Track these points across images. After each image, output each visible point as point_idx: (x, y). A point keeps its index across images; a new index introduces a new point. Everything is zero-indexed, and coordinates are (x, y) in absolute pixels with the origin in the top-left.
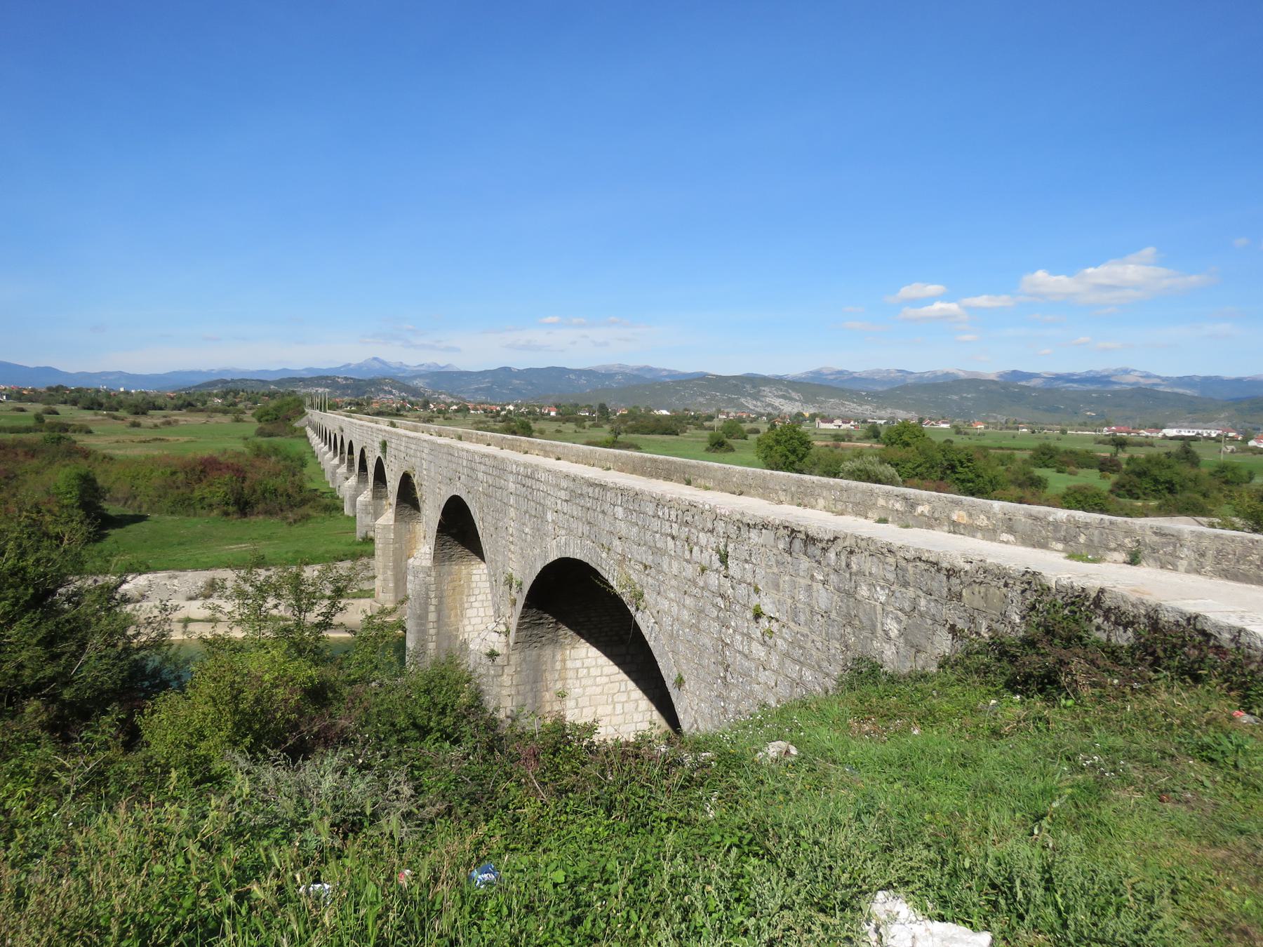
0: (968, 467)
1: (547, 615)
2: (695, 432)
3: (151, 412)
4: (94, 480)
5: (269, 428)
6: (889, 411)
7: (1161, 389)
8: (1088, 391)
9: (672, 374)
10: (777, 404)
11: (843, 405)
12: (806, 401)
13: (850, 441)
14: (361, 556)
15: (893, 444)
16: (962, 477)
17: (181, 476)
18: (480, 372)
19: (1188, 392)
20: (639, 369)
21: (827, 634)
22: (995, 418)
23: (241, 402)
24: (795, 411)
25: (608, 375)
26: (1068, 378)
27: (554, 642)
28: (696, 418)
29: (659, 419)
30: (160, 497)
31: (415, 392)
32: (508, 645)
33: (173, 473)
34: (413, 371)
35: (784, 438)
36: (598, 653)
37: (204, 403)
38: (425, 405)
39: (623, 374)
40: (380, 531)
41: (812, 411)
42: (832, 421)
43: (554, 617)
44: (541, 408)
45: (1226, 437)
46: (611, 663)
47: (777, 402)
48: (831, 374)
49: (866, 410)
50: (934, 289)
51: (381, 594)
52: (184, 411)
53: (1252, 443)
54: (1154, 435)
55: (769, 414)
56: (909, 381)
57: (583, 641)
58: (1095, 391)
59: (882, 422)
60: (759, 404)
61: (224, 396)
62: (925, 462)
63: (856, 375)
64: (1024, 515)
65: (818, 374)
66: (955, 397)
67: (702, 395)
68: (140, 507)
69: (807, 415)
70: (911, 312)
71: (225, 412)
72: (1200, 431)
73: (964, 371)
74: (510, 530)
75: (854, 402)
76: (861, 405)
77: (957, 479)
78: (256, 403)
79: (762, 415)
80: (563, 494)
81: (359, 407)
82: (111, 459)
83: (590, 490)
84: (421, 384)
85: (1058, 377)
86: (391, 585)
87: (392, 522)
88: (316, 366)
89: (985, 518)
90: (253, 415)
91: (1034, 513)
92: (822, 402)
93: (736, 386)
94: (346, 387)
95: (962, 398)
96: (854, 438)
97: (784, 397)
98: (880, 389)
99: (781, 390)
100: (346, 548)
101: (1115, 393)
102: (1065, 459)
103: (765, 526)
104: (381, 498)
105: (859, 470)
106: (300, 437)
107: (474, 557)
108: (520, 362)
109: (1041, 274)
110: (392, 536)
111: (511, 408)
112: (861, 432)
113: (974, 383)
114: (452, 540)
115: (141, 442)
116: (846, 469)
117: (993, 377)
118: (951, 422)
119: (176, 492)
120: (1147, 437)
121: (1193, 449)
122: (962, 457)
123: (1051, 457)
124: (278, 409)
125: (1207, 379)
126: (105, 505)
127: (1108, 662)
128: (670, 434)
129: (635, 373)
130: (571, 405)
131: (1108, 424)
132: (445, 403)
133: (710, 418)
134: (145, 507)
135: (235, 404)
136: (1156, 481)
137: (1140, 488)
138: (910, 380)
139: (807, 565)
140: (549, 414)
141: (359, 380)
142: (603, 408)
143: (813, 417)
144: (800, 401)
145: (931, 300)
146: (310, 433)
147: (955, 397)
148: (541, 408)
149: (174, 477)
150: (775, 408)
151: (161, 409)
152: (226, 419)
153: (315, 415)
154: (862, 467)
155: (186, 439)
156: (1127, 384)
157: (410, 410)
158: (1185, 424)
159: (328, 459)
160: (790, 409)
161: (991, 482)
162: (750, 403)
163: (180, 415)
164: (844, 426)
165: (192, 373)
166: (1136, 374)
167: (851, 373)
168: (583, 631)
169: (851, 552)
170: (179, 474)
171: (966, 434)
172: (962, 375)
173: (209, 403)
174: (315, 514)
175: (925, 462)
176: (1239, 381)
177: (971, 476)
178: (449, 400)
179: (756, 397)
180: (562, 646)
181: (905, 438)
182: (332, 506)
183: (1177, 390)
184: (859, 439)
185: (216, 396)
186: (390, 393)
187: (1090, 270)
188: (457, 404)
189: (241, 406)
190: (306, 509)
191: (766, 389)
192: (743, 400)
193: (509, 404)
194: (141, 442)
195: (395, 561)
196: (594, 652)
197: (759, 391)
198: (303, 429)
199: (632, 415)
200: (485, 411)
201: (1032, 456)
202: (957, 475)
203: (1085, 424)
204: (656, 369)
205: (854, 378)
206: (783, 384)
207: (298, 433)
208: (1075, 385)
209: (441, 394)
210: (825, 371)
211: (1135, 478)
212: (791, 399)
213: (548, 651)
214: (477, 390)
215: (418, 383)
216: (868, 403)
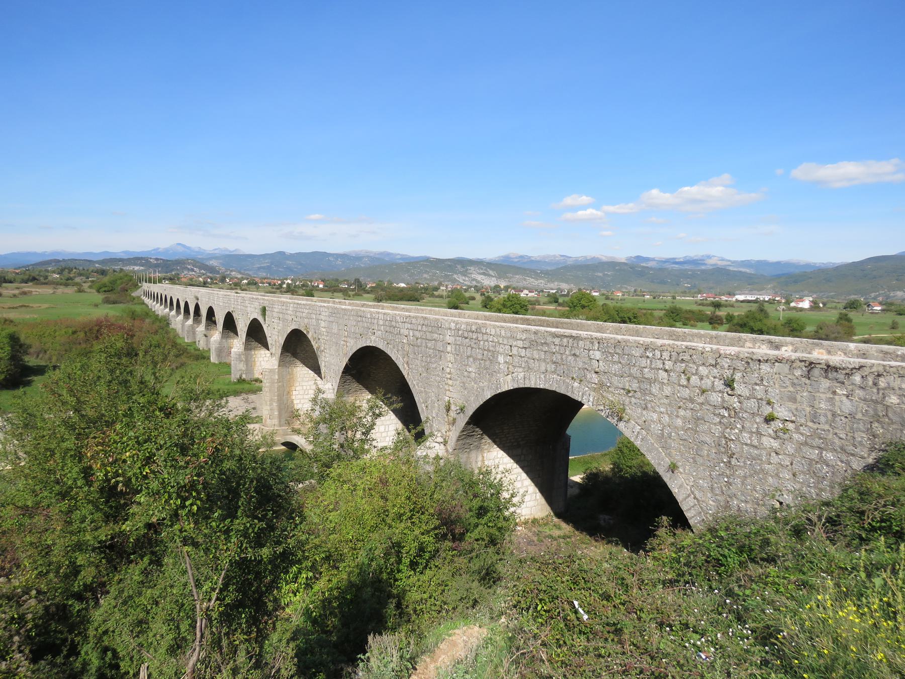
1: (477, 429)
2: (430, 299)
3: (4, 285)
4: (18, 339)
5: (112, 296)
6: (556, 283)
7: (731, 268)
8: (686, 269)
9: (404, 258)
10: (479, 279)
11: (525, 280)
12: (499, 277)
13: (539, 305)
14: (241, 392)
15: (575, 306)
17: (81, 335)
18: (261, 255)
19: (748, 271)
20: (381, 253)
21: (852, 428)
22: (626, 288)
23: (75, 277)
24: (493, 284)
25: (358, 258)
26: (674, 261)
27: (478, 448)
28: (426, 289)
29: (402, 290)
30: (66, 351)
31: (212, 269)
32: (447, 451)
33: (74, 333)
34: (209, 254)
35: (509, 304)
36: (505, 455)
37: (46, 277)
38: (223, 280)
39: (368, 257)
40: (267, 373)
43: (482, 430)
44: (311, 282)
45: (774, 300)
46: (512, 461)
47: (479, 278)
49: (541, 283)
50: (585, 199)
51: (268, 420)
52: (30, 284)
53: (793, 304)
54: (730, 299)
56: (569, 263)
57: (495, 446)
58: (691, 270)
59: (554, 291)
60: (467, 279)
61: (61, 272)
63: (533, 259)
64: (877, 352)
65: (507, 258)
66: (600, 274)
67: (426, 272)
68: (50, 359)
69: (502, 287)
70: (569, 215)
71: (66, 285)
74: (448, 370)
76: (537, 280)
78: (88, 278)
79: (471, 287)
80: (520, 344)
81: (173, 280)
82: (11, 321)
83: (557, 341)
84: (215, 264)
85: (667, 261)
86: (276, 413)
87: (276, 367)
88: (131, 250)
89: (842, 354)
90: (90, 287)
91: (883, 350)
92: (511, 278)
93: (450, 266)
94: (157, 266)
95: (604, 275)
97: (484, 274)
98: (549, 269)
100: (227, 387)
101: (703, 271)
102: (688, 316)
103: (767, 361)
104: (251, 349)
106: (139, 304)
107: (365, 390)
108: (292, 247)
109: (655, 192)
110: (277, 377)
111: (290, 282)
112: (544, 300)
113: (612, 265)
114: (351, 378)
115: (10, 308)
117: (623, 261)
118: (599, 291)
119: (79, 347)
120: (727, 301)
121: (765, 308)
124: (113, 282)
125: (758, 262)
126: (26, 358)
128: (414, 301)
129: (377, 256)
130: (333, 280)
131: (700, 292)
132: (236, 278)
133: (436, 289)
134: (54, 359)
135: (71, 279)
138: (570, 262)
139: (828, 385)
140: (318, 286)
141: (168, 261)
142: (357, 281)
145: (584, 207)
146: (147, 301)
147: (600, 274)
148: (311, 282)
149: (76, 336)
150: (478, 282)
151: (11, 282)
152: (70, 290)
153: (146, 286)
155: (46, 306)
156: (711, 265)
157: (212, 283)
159: (178, 322)
160: (488, 282)
162: (461, 279)
163: (28, 287)
164: (531, 294)
165: (28, 254)
166: (715, 258)
167: (530, 257)
168: (497, 440)
169: (879, 375)
170: (79, 333)
171: (612, 299)
172: (604, 259)
173: (49, 278)
174: (190, 362)
176: (778, 263)
178: (239, 276)
179: (465, 274)
180: (482, 451)
181: (583, 302)
182: (202, 356)
184: (545, 304)
185: (54, 272)
186: (193, 270)
187: (686, 189)
188: (247, 279)
189: (78, 280)
190: (183, 359)
192: (455, 276)
193: (287, 279)
194: (10, 308)
195: (278, 396)
196: (501, 453)
197: (467, 270)
198: (139, 297)
199: (379, 287)
200: (270, 284)
204: (392, 254)
205: (531, 261)
206: (484, 266)
207: (135, 301)
208: (677, 266)
209: (232, 271)
210: (512, 256)
212: (489, 275)
213: (473, 454)
214: (259, 268)
215: (213, 263)
216: (541, 278)
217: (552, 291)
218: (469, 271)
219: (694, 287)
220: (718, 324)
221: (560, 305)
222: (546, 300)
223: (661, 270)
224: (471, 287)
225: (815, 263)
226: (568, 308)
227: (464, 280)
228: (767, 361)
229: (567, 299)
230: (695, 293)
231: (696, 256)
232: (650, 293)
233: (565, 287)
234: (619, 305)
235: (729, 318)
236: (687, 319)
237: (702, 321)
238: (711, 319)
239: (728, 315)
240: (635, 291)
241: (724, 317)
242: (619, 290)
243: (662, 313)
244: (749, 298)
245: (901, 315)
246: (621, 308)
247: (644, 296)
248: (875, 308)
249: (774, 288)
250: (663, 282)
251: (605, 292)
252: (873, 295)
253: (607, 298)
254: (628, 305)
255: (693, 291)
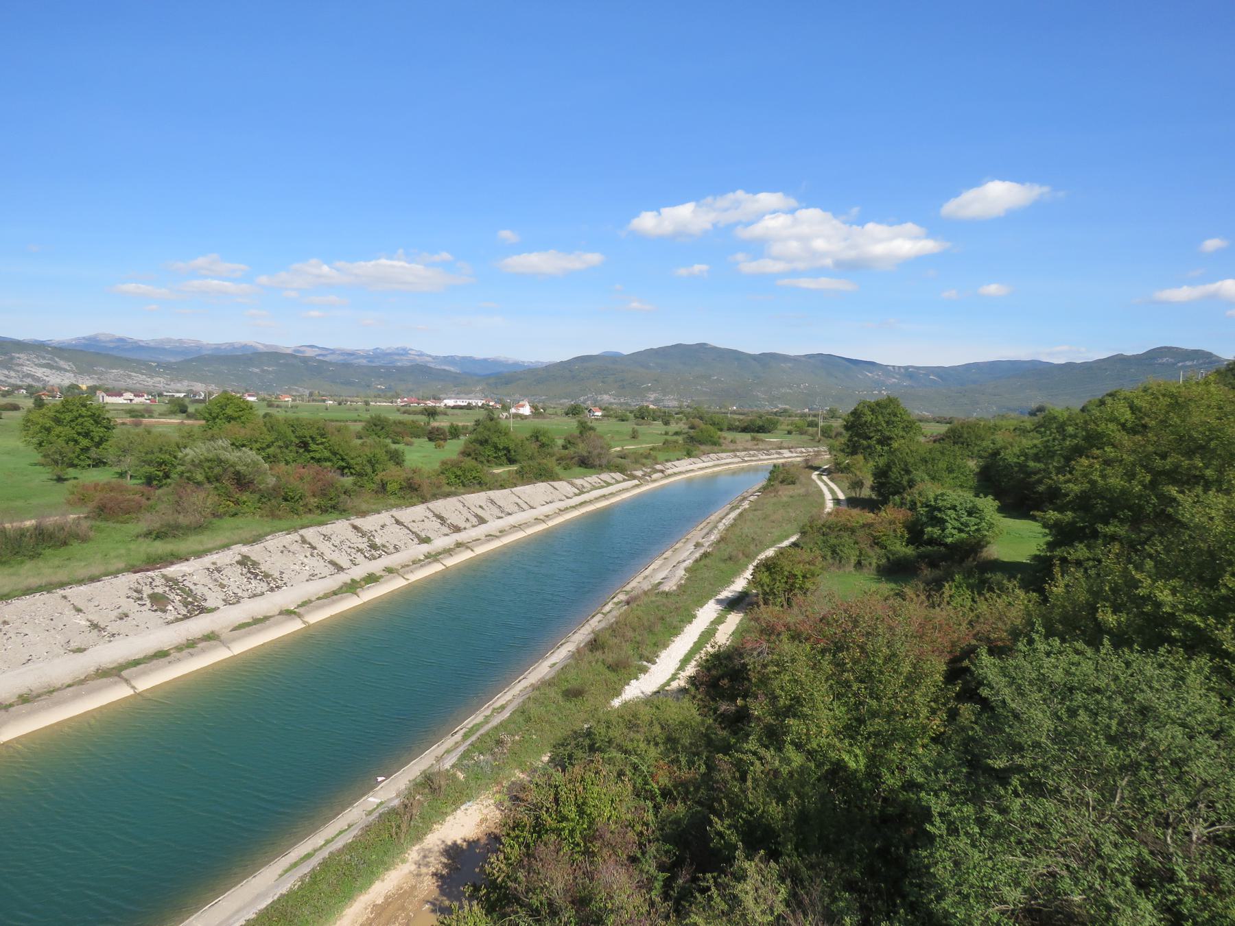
0: (322, 443)
6: (186, 383)
7: (432, 365)
11: (130, 377)
12: (81, 371)
13: (151, 417)
15: (214, 419)
16: (317, 455)
19: (452, 369)
24: (66, 383)
35: (68, 416)
41: (91, 383)
42: (120, 395)
45: (488, 405)
47: (39, 372)
48: (111, 341)
49: (159, 382)
54: (438, 405)
55: (28, 388)
59: (182, 395)
60: (12, 374)
62: (277, 440)
63: (142, 344)
72: (470, 401)
73: (263, 345)
75: (143, 374)
76: (151, 377)
77: (312, 458)
79: (20, 387)
92: (102, 373)
95: (263, 371)
96: (156, 414)
98: (172, 360)
99: (44, 358)
105: (208, 461)
112: (160, 407)
113: (273, 356)
116: (188, 458)
122: (314, 432)
123: (383, 428)
125: (464, 358)
127: (745, 758)
131: (398, 396)
136: (496, 448)
137: (484, 456)
143: (93, 390)
144: (71, 371)
150: (38, 379)
154: (211, 456)
158: (453, 396)
161: (369, 461)
164: (137, 400)
172: (261, 348)
175: (277, 440)
176: (485, 360)
177: (327, 454)
181: (229, 411)
183: (447, 368)
184: (162, 415)
191: (21, 355)
201: (364, 428)
202: (312, 454)
203: (379, 396)
205: (138, 347)
206: (48, 352)
211: (478, 446)
212: (59, 369)
216: (159, 374)
217: (177, 395)
218: (18, 361)
219: (389, 388)
220: (441, 439)
221: (190, 416)
222: (164, 408)
223: (346, 365)
224: (20, 387)
225: (523, 362)
226: (203, 422)
227: (7, 376)
228: (195, 529)
229: (201, 407)
230: (393, 397)
231: (536, 362)
232: (332, 396)
233: (200, 388)
234: (291, 415)
235: (453, 431)
236: (398, 434)
237: (418, 436)
238: (431, 433)
239: (452, 426)
240: (311, 394)
241: (447, 431)
242: (288, 393)
243: (358, 427)
244: (460, 403)
245: (623, 420)
246: (298, 419)
247: (324, 401)
248: (596, 414)
249: (482, 391)
250: (348, 383)
251: (266, 397)
252: (582, 399)
253: (270, 405)
254: (304, 415)
255: (389, 394)
